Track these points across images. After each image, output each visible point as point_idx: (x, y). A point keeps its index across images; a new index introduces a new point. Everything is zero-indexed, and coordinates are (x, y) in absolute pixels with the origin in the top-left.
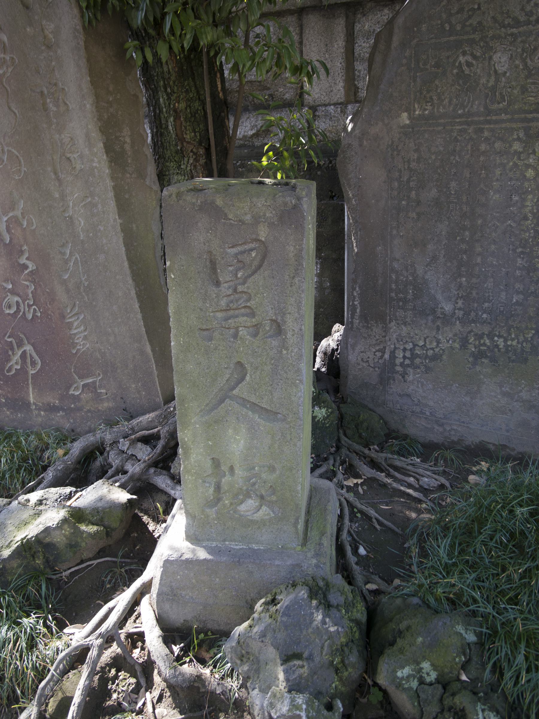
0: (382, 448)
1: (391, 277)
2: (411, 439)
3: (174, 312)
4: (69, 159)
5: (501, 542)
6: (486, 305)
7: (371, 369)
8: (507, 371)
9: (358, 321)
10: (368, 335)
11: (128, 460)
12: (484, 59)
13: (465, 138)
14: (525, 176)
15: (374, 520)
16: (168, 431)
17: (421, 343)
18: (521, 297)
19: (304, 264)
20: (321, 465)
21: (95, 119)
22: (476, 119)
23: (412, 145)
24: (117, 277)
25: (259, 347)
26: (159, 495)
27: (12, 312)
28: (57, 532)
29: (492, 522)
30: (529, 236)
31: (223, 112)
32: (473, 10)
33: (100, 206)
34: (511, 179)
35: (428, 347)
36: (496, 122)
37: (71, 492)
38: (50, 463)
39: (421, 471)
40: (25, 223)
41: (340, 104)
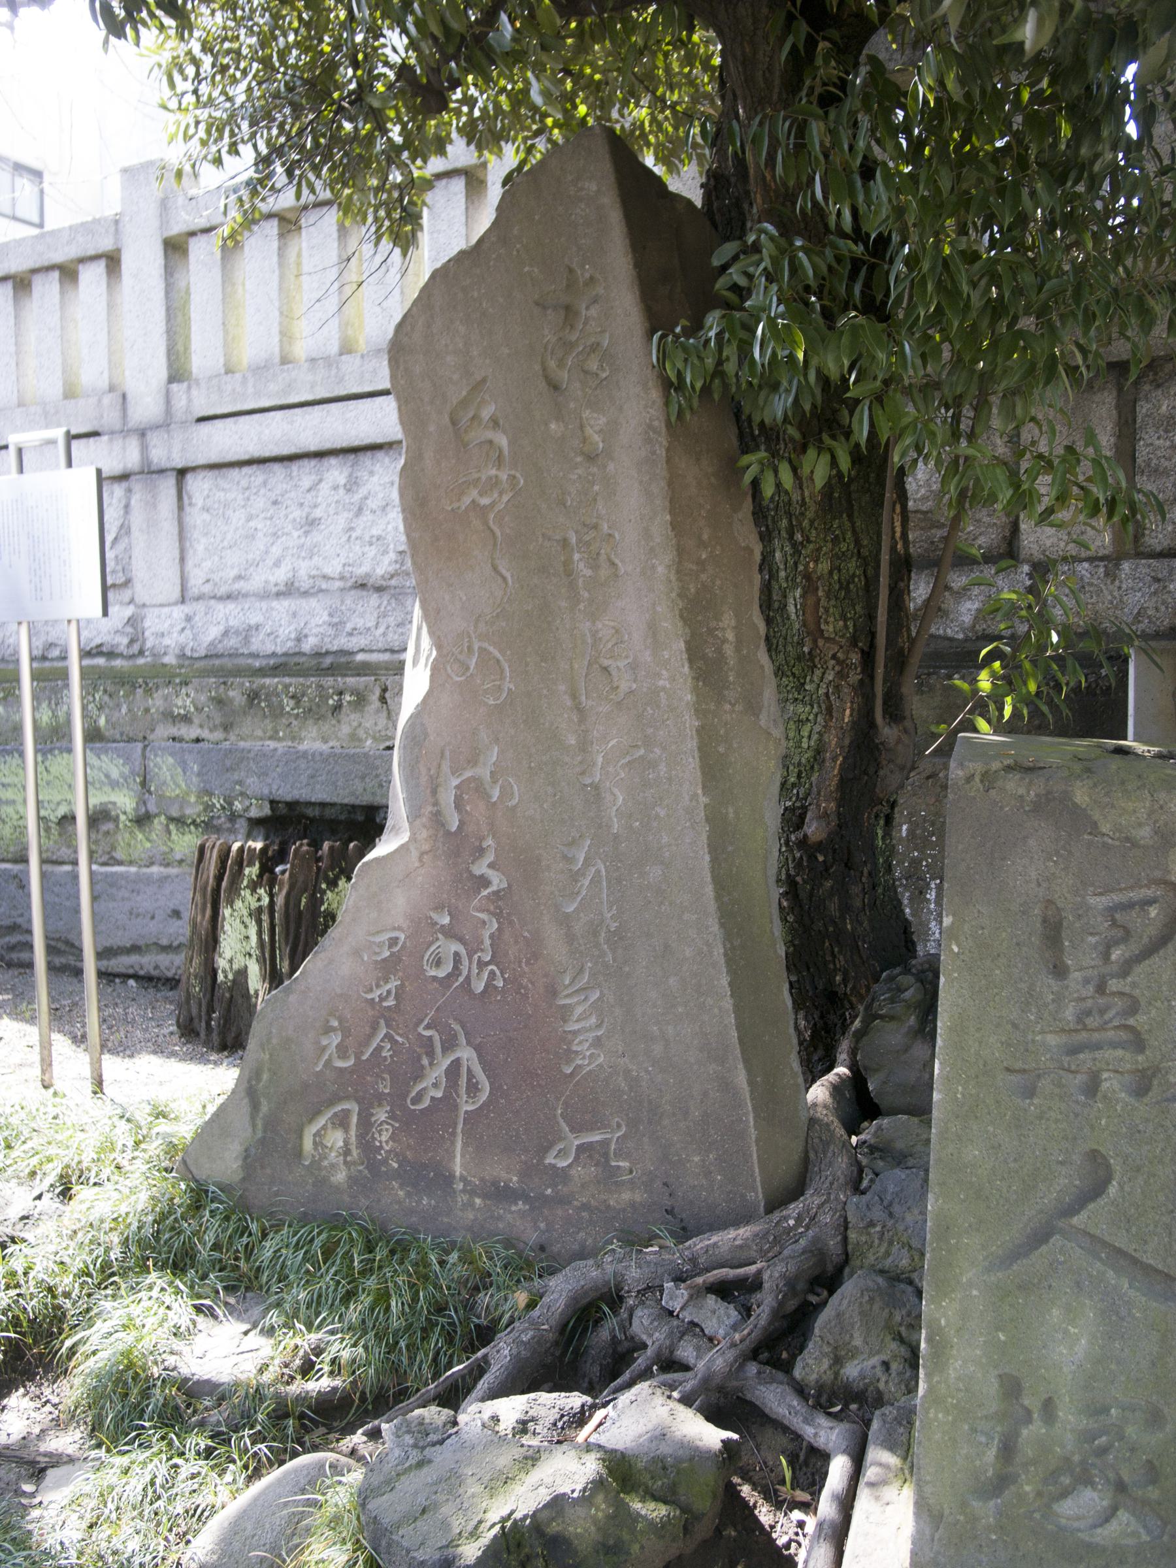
3: (950, 1028)
4: (605, 669)
11: (683, 1334)
16: (783, 1276)
21: (673, 595)
24: (686, 916)
25: (1147, 1120)
26: (769, 1431)
27: (441, 974)
28: (581, 1511)
33: (663, 768)
37: (583, 1406)
38: (496, 1321)
40: (496, 794)
41: (1102, 559)
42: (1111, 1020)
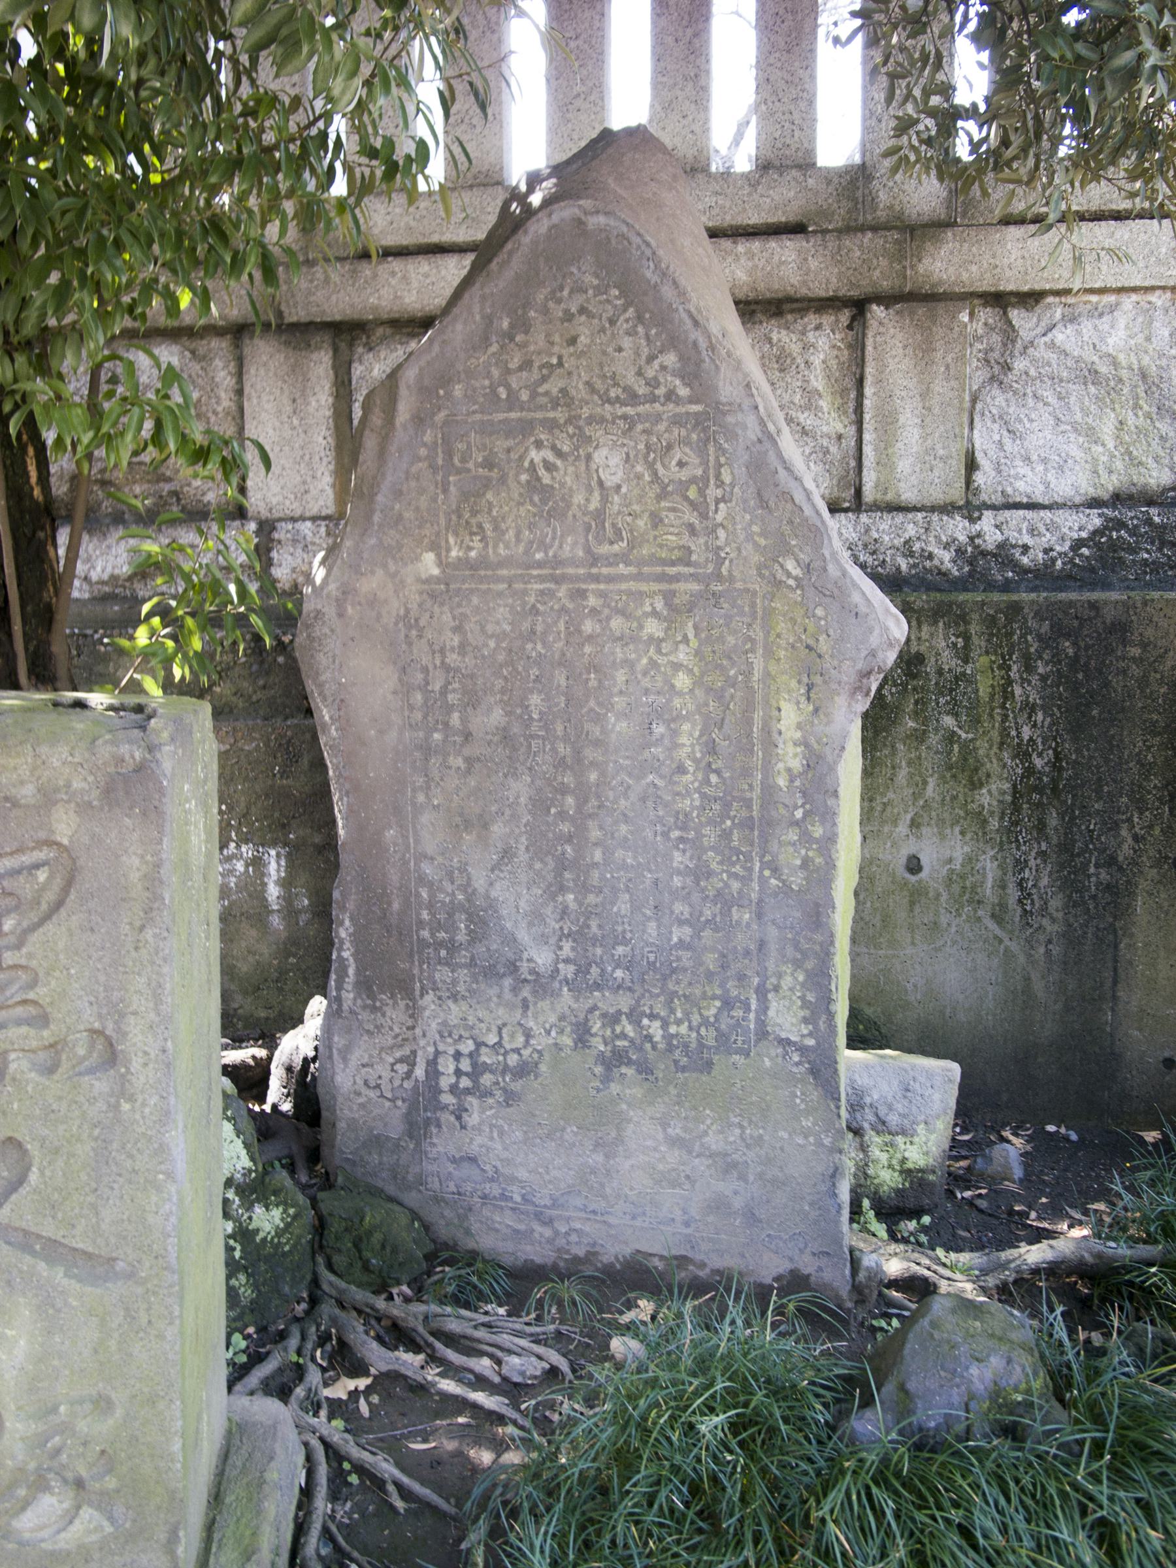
0: (420, 1290)
1: (418, 895)
2: (485, 1261)
5: (672, 1511)
6: (620, 950)
7: (387, 1104)
8: (673, 1091)
9: (351, 995)
10: (376, 1027)
12: (578, 458)
13: (552, 608)
14: (673, 686)
15: (391, 1488)
17: (492, 1039)
18: (687, 931)
19: (167, 896)
20: (268, 1353)
22: (571, 571)
23: (447, 618)
25: (60, 1098)
29: (650, 1460)
30: (693, 808)
31: (43, 528)
32: (549, 365)
34: (647, 692)
35: (508, 1047)
36: (610, 579)
39: (505, 1339)
42: (12, 996)
